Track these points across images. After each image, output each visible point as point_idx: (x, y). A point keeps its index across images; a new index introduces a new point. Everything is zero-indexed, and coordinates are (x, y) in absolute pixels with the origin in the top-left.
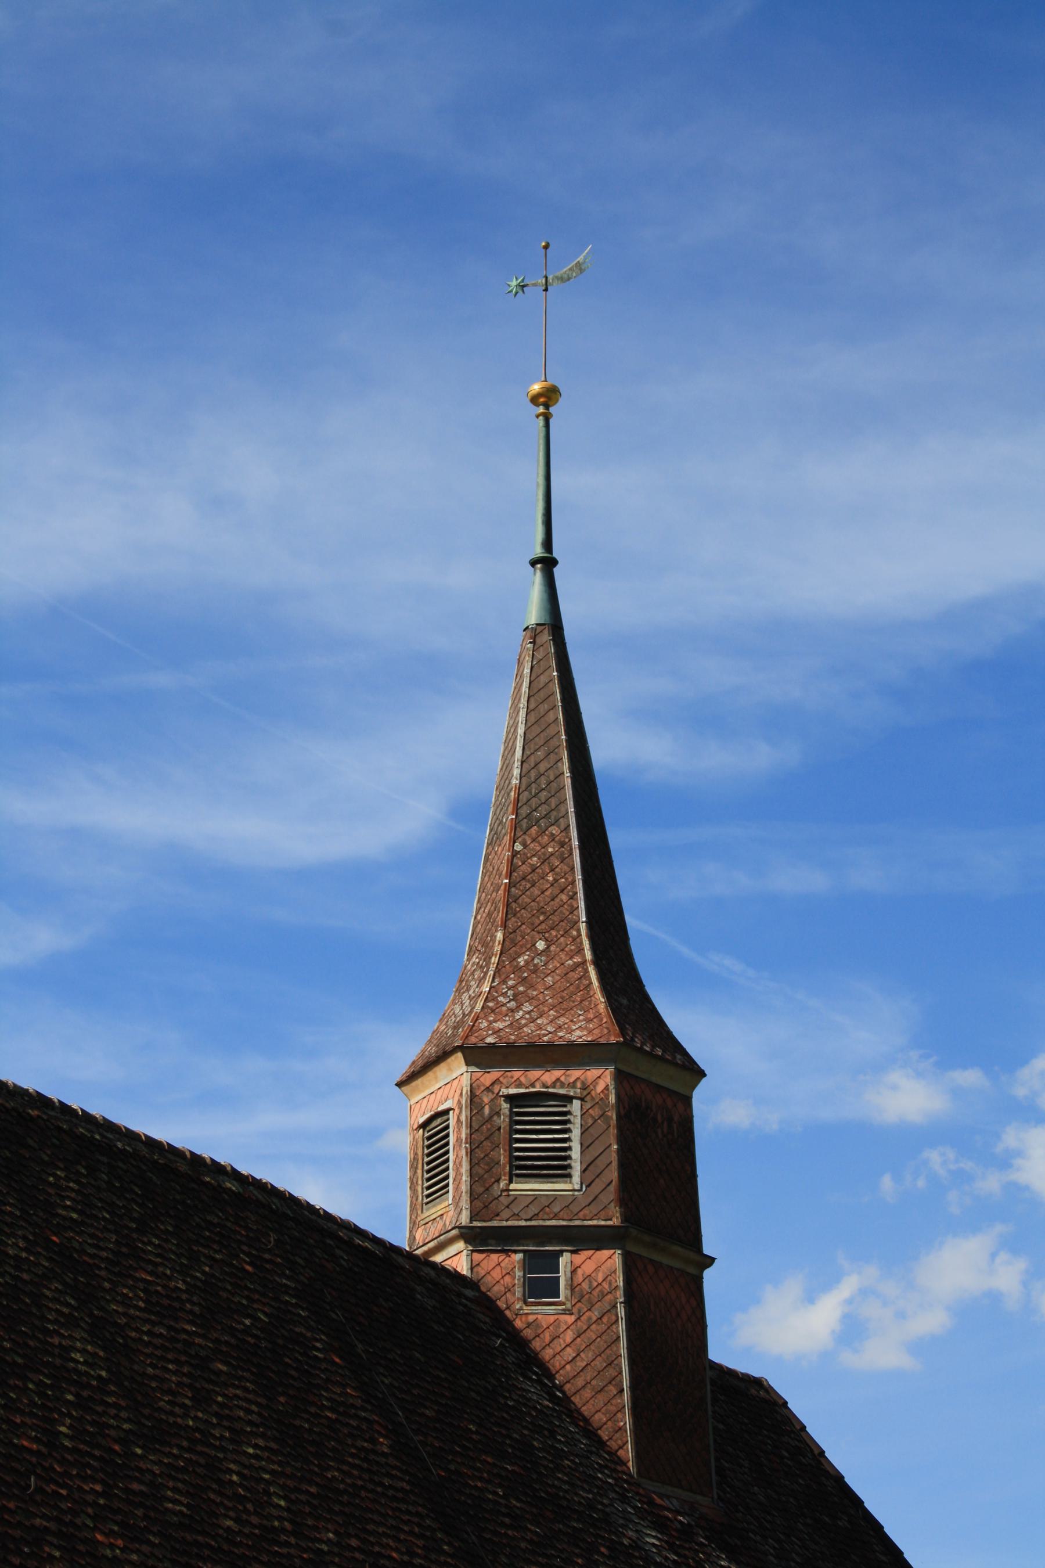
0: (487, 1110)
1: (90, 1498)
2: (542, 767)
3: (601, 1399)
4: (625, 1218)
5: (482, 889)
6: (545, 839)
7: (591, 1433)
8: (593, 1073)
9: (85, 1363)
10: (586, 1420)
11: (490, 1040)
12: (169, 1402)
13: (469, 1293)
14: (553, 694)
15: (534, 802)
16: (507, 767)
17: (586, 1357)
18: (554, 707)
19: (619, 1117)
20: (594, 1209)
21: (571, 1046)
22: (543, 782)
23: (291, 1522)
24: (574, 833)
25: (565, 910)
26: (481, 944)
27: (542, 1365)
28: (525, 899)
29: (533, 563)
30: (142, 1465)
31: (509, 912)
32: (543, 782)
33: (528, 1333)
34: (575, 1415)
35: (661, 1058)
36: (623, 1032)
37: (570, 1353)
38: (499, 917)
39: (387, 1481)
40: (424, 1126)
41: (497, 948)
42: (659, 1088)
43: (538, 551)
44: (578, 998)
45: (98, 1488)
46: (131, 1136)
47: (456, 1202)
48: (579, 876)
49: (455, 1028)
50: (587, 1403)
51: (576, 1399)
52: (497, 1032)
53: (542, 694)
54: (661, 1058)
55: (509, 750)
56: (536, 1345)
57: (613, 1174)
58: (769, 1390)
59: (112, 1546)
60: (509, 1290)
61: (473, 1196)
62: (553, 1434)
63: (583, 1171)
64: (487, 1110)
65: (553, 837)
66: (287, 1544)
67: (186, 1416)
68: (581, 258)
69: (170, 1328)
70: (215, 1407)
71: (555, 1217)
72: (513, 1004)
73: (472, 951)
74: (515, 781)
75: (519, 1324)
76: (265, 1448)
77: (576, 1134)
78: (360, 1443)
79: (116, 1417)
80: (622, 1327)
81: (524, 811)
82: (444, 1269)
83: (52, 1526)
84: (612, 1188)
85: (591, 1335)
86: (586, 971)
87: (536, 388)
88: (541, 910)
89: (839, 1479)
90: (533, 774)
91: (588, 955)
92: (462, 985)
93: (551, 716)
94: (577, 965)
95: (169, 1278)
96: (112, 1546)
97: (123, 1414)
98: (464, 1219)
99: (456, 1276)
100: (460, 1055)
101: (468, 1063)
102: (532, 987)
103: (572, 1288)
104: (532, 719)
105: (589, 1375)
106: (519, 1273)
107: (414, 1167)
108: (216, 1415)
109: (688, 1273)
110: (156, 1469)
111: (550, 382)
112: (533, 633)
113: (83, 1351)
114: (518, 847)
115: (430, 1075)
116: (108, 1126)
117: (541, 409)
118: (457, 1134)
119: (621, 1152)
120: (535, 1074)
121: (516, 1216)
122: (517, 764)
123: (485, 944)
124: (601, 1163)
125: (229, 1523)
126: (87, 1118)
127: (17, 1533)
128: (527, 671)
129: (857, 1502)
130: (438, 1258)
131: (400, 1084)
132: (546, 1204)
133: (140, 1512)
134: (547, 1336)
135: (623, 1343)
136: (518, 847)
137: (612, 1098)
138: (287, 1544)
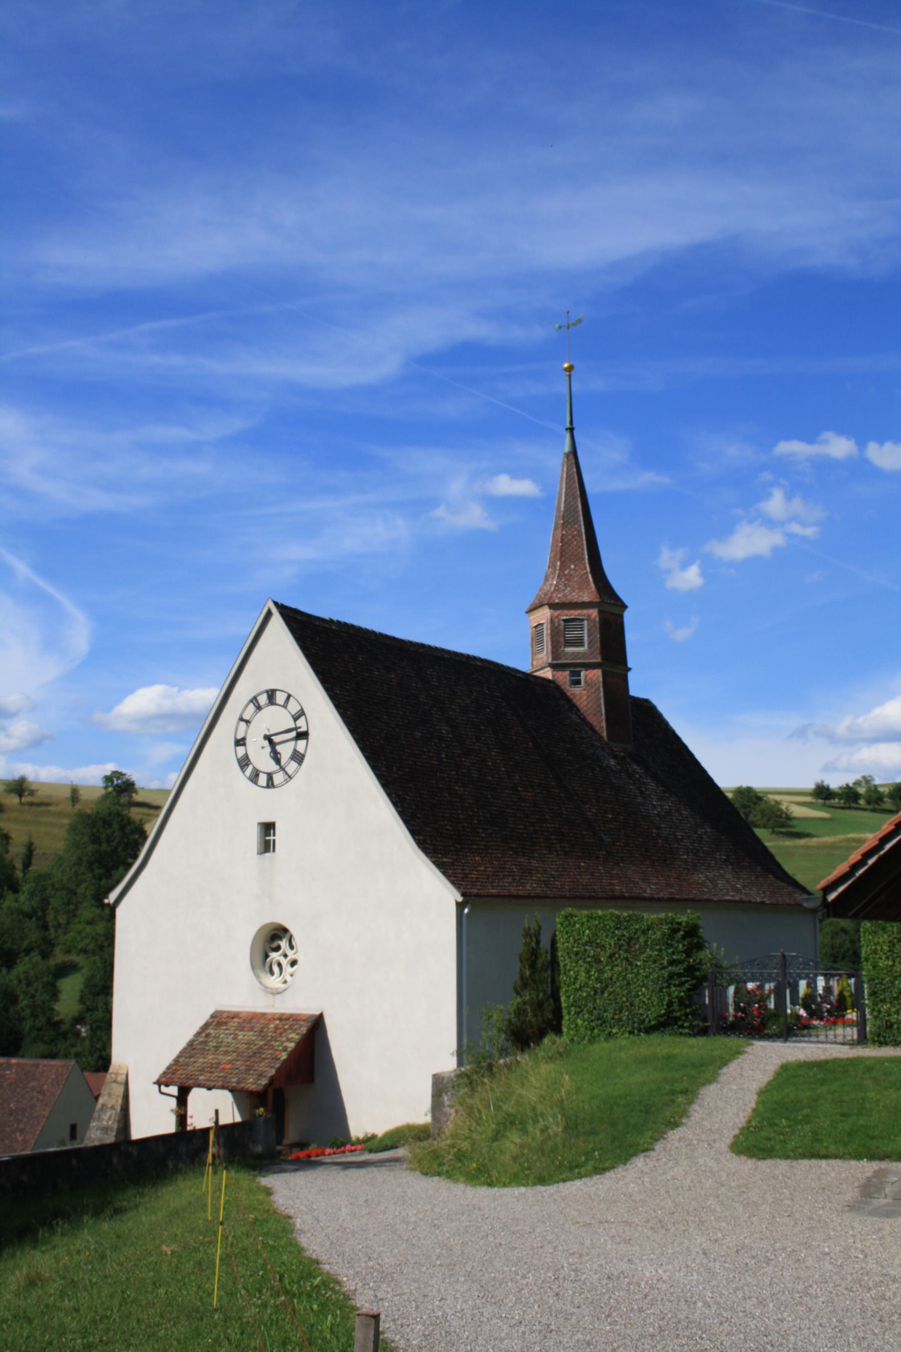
0: (556, 624)
2: (572, 503)
4: (603, 659)
6: (573, 529)
7: (592, 728)
8: (591, 611)
11: (557, 601)
12: (465, 870)
14: (574, 477)
15: (569, 516)
16: (559, 503)
17: (591, 704)
18: (575, 482)
22: (572, 509)
26: (552, 565)
28: (567, 550)
29: (567, 429)
31: (562, 555)
32: (572, 509)
33: (571, 697)
35: (613, 604)
37: (585, 703)
38: (558, 556)
40: (536, 627)
41: (558, 568)
42: (613, 614)
43: (568, 425)
44: (585, 585)
47: (547, 654)
48: (585, 543)
50: (591, 719)
52: (559, 598)
54: (613, 604)
55: (560, 498)
56: (574, 701)
60: (565, 683)
61: (553, 653)
63: (589, 644)
64: (556, 624)
65: (576, 529)
71: (580, 659)
73: (549, 567)
74: (562, 509)
75: (569, 694)
80: (602, 695)
81: (566, 519)
85: (592, 697)
86: (587, 577)
87: (566, 365)
88: (572, 555)
91: (588, 569)
92: (546, 579)
98: (550, 660)
99: (548, 681)
103: (586, 682)
106: (568, 678)
109: (569, 1180)
111: (571, 363)
112: (567, 455)
114: (564, 532)
118: (546, 632)
120: (572, 612)
121: (567, 659)
131: (527, 612)
132: (576, 655)
134: (578, 698)
137: (597, 619)
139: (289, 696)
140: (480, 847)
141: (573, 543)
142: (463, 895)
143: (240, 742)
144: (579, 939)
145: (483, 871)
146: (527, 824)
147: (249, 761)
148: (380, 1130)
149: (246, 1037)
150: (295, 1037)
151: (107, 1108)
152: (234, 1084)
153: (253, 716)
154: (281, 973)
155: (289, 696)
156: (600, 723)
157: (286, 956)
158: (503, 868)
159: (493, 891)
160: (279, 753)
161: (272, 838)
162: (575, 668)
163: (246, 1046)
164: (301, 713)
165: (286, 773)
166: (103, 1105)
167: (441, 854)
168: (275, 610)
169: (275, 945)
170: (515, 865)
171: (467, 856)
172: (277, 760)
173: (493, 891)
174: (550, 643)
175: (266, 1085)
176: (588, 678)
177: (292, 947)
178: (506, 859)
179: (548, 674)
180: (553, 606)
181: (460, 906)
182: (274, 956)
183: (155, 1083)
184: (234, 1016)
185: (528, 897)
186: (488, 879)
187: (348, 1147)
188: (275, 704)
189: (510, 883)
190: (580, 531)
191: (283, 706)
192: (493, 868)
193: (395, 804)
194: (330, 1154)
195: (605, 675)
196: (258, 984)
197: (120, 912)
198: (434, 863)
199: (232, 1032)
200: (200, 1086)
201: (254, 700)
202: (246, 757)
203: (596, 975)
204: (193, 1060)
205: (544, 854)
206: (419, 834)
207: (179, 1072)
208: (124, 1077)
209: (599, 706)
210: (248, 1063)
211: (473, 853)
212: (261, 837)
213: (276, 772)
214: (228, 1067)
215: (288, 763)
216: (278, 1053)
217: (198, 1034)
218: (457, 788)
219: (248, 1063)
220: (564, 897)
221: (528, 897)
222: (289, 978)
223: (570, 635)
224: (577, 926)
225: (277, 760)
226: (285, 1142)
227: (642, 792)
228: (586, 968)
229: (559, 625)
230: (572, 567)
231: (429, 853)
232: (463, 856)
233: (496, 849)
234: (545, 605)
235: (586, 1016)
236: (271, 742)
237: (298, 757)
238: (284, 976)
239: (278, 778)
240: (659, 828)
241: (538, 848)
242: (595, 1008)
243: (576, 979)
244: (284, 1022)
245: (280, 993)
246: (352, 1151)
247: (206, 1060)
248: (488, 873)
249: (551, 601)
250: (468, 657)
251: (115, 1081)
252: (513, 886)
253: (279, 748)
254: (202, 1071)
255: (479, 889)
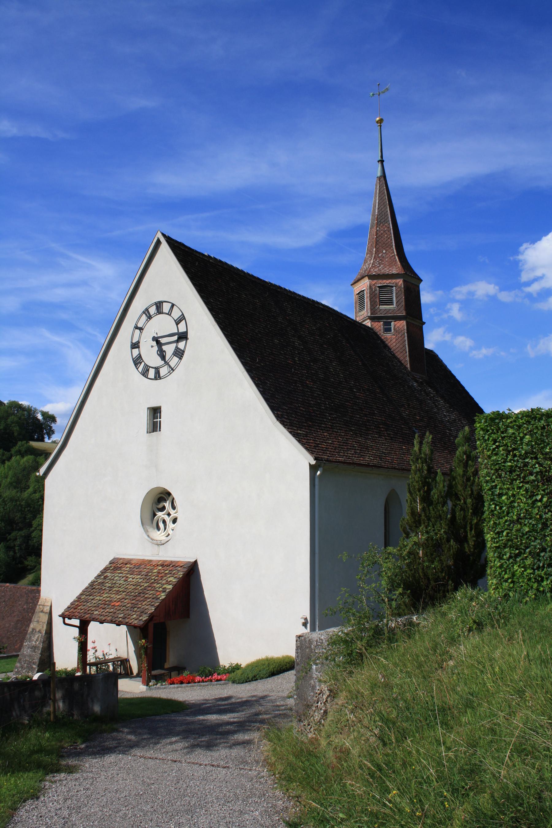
0: (374, 290)
1: (304, 374)
2: (383, 210)
3: (402, 354)
4: (407, 313)
5: (369, 239)
6: (384, 227)
8: (398, 280)
9: (298, 345)
10: (399, 359)
11: (374, 273)
13: (372, 331)
14: (385, 192)
15: (381, 218)
16: (374, 210)
17: (398, 345)
18: (385, 195)
19: (404, 291)
20: (399, 312)
21: (393, 274)
23: (345, 380)
24: (391, 225)
25: (390, 243)
27: (388, 347)
29: (378, 161)
30: (313, 367)
31: (376, 244)
32: (383, 213)
33: (385, 340)
34: (396, 357)
36: (405, 271)
37: (394, 344)
39: (362, 371)
40: (358, 294)
41: (374, 253)
42: (413, 284)
44: (394, 263)
45: (306, 372)
46: (299, 295)
47: (367, 311)
48: (393, 235)
49: (365, 271)
50: (399, 355)
51: (396, 354)
52: (375, 272)
53: (382, 193)
56: (387, 342)
57: (403, 303)
58: (434, 353)
59: (311, 384)
60: (380, 330)
61: (371, 310)
62: (393, 362)
63: (396, 303)
64: (374, 290)
65: (386, 226)
66: (344, 384)
67: (320, 357)
68: (387, 87)
69: (314, 338)
70: (325, 355)
71: (390, 314)
72: (378, 265)
74: (376, 213)
75: (383, 338)
76: (337, 364)
77: (394, 295)
78: (355, 363)
79: (306, 357)
80: (406, 338)
81: (379, 220)
82: (366, 326)
83: (298, 379)
84: (403, 307)
85: (399, 340)
87: (378, 119)
88: (384, 243)
89: (450, 372)
90: (381, 211)
91: (395, 253)
92: (365, 261)
93: (384, 197)
94: (392, 256)
95: (312, 327)
96: (311, 384)
97: (308, 356)
98: (369, 315)
99: (368, 327)
100: (367, 277)
101: (369, 279)
102: (383, 261)
103: (395, 329)
104: (380, 199)
105: (399, 349)
106: (382, 327)
107: (356, 304)
108: (326, 356)
110: (316, 368)
111: (381, 118)
112: (379, 178)
113: (297, 342)
114: (378, 229)
115: (359, 282)
116: (294, 293)
117: (379, 124)
118: (367, 295)
119: (405, 299)
120: (384, 281)
121: (381, 314)
122: (377, 209)
123: (371, 252)
124: (401, 301)
125: (332, 380)
126: (290, 291)
127: (291, 381)
128: (378, 187)
129: (454, 377)
130: (364, 323)
131: (351, 285)
133: (315, 377)
134: (389, 341)
135: (407, 342)
136: (378, 229)
137: (403, 286)
138: (344, 384)
139: (173, 305)
140: (328, 426)
141: (384, 235)
142: (315, 459)
143: (135, 345)
144: (514, 449)
145: (331, 443)
146: (362, 415)
147: (142, 359)
148: (244, 660)
149: (134, 580)
150: (173, 580)
151: (36, 632)
152: (120, 619)
153: (145, 324)
154: (165, 529)
155: (173, 305)
156: (406, 359)
157: (169, 515)
158: (346, 443)
159: (341, 459)
160: (165, 351)
161: (159, 420)
162: (387, 320)
163: (134, 587)
164: (182, 318)
165: (170, 366)
166: (33, 629)
167: (296, 427)
168: (162, 240)
169: (161, 506)
170: (355, 442)
171: (318, 432)
172: (163, 357)
173: (341, 459)
174: (369, 303)
175: (146, 620)
176: (396, 327)
177: (174, 508)
178: (348, 437)
179: (368, 323)
180: (371, 277)
181: (313, 469)
182: (160, 514)
183: (60, 616)
184: (127, 562)
185: (368, 466)
186: (335, 449)
187: (215, 676)
188: (162, 313)
189: (353, 454)
190: (389, 228)
191: (168, 314)
192: (338, 442)
193: (257, 385)
194: (199, 682)
195: (408, 324)
196: (146, 537)
197: (48, 482)
198: (290, 432)
199: (124, 575)
200: (95, 620)
201: (146, 312)
202: (140, 356)
203: (545, 499)
204: (91, 597)
205: (376, 437)
206: (278, 410)
207: (79, 608)
208: (48, 608)
209: (404, 346)
210: (133, 601)
211: (322, 430)
212: (150, 419)
213: (162, 366)
214: (117, 604)
215: (171, 358)
216: (158, 593)
217: (99, 576)
218: (308, 382)
219: (133, 601)
220: (395, 468)
221: (368, 466)
222: (171, 532)
223: (384, 297)
224: (511, 431)
225: (163, 357)
226: (167, 666)
227: (436, 406)
228: (527, 490)
229: (376, 290)
230: (384, 251)
231: (287, 425)
232: (314, 431)
233: (340, 429)
234: (365, 276)
235: (528, 562)
236: (158, 342)
237: (179, 354)
238: (168, 531)
239: (164, 371)
240: (450, 430)
241: (371, 432)
242: (544, 550)
243: (511, 506)
244: (165, 568)
245: (163, 544)
246: (218, 680)
247: (101, 598)
248: (335, 445)
249: (370, 273)
250: (313, 301)
251: (42, 611)
252: (355, 457)
253: (164, 348)
254: (97, 607)
255: (328, 456)
